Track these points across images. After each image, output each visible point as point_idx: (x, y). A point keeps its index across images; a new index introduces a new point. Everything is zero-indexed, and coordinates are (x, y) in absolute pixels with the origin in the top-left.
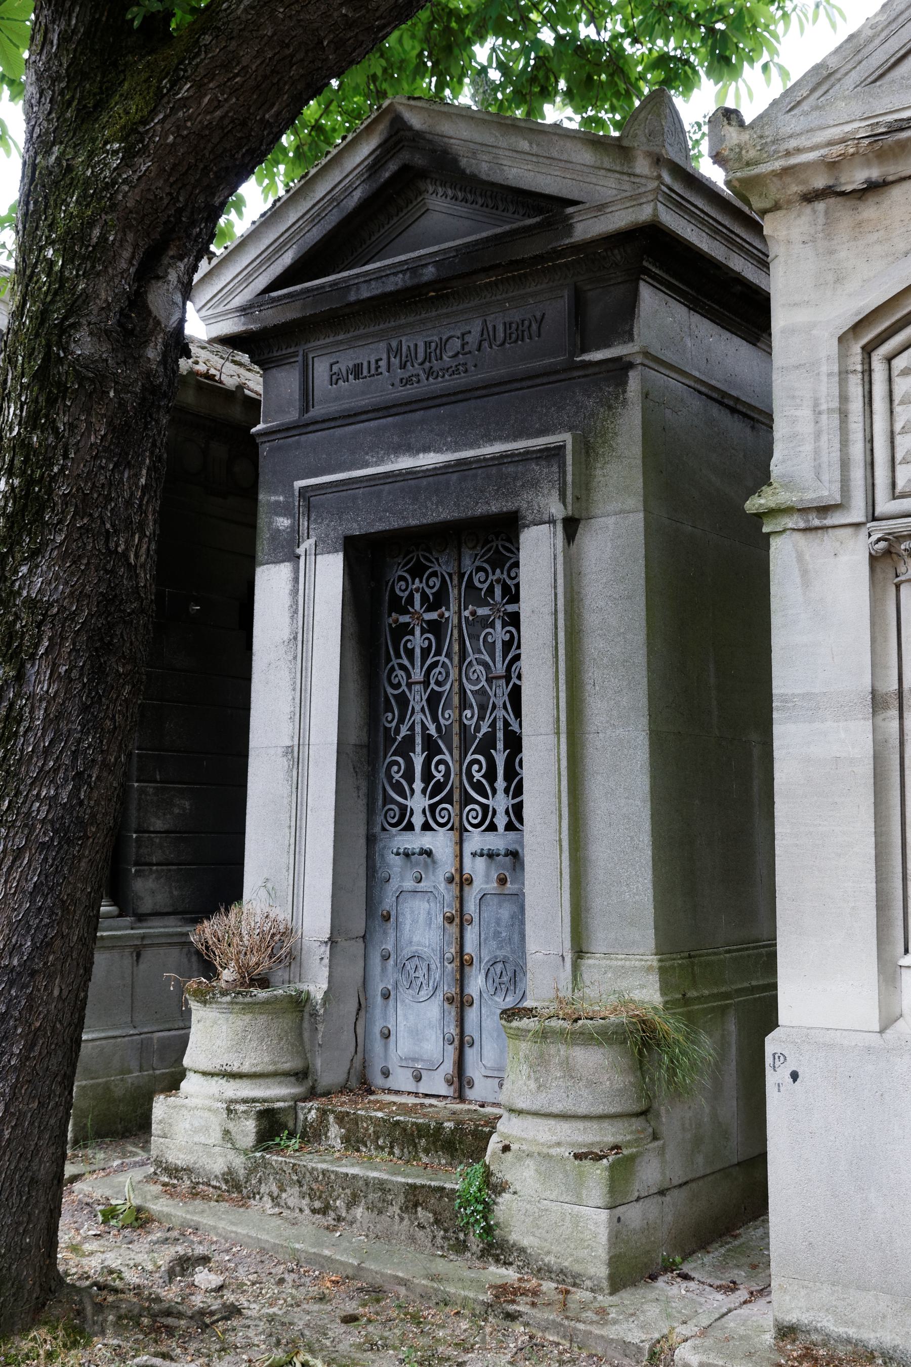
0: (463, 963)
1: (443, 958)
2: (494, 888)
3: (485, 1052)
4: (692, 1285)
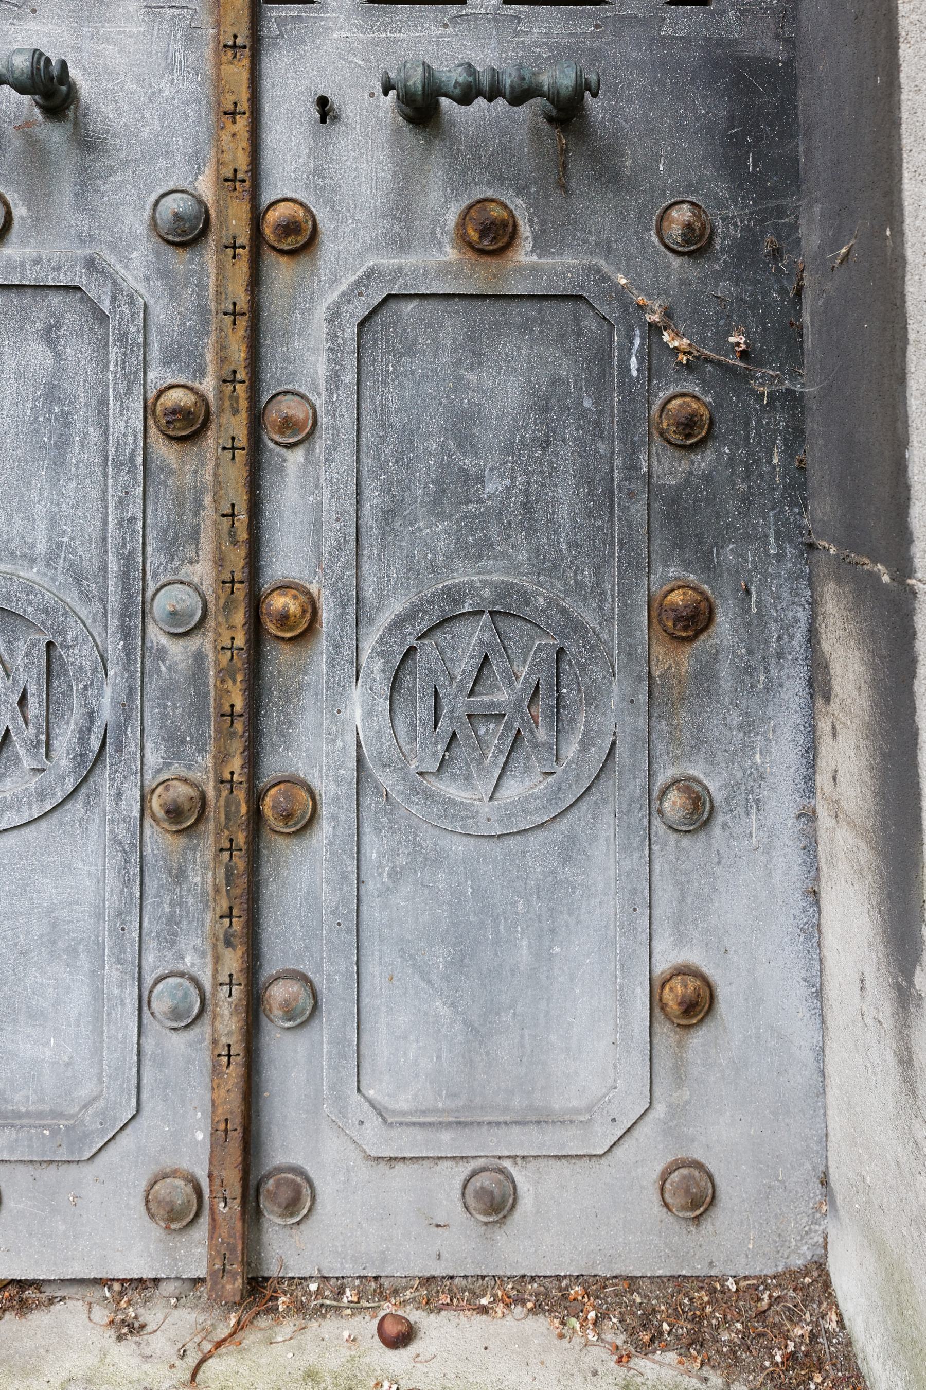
0: (263, 631)
1: (136, 612)
2: (442, 272)
3: (380, 1045)
4: (839, 767)
